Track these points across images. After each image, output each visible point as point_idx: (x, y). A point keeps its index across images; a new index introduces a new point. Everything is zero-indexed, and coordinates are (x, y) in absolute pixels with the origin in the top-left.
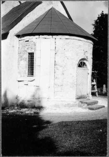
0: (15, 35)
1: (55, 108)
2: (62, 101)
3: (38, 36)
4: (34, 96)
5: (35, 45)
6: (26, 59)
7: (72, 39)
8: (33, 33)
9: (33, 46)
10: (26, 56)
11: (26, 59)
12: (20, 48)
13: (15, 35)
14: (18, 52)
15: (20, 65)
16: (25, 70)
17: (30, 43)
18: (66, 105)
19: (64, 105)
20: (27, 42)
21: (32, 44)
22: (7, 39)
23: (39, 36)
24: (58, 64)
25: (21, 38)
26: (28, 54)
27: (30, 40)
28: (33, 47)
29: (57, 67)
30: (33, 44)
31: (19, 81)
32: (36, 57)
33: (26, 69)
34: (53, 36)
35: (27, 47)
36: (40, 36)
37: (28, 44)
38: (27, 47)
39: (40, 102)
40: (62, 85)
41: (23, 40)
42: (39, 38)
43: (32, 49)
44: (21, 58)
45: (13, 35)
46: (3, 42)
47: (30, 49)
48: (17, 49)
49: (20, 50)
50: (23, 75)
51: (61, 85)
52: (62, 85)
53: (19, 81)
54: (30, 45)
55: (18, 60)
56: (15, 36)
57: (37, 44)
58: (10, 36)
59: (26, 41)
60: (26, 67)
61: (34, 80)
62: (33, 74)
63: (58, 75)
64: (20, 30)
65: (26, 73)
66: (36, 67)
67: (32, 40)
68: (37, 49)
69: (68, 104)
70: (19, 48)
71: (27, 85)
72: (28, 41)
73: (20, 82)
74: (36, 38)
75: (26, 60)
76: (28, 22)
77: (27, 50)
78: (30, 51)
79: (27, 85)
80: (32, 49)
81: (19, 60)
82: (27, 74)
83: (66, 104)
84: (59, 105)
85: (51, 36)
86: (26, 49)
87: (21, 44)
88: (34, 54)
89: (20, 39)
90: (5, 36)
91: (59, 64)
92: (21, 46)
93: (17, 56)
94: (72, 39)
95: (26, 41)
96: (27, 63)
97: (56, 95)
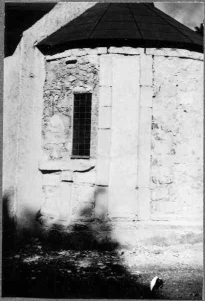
0: (36, 44)
1: (156, 248)
2: (172, 227)
3: (106, 48)
4: (87, 212)
5: (95, 73)
6: (67, 111)
7: (194, 59)
8: (91, 37)
9: (88, 75)
10: (69, 102)
11: (67, 111)
12: (48, 83)
13: (36, 46)
14: (44, 91)
15: (49, 128)
16: (64, 141)
17: (82, 67)
18: (183, 237)
19: (179, 239)
20: (70, 66)
21: (85, 69)
22: (14, 54)
23: (108, 48)
24: (159, 126)
25: (51, 55)
26: (73, 96)
27: (80, 60)
28: (88, 78)
29: (157, 134)
30: (90, 70)
31: (45, 172)
32: (97, 108)
33: (67, 138)
34: (147, 49)
35: (71, 78)
36: (111, 48)
37: (72, 71)
38: (71, 78)
39: (107, 229)
40: (171, 182)
41: (59, 59)
42: (108, 53)
43: (85, 82)
44: (51, 108)
45: (32, 45)
46: (8, 61)
47: (81, 83)
48: (39, 83)
49: (48, 87)
50: (55, 155)
51: (169, 182)
52: (171, 182)
53: (45, 172)
54: (81, 72)
55: (44, 114)
56: (36, 48)
57: (102, 72)
58: (25, 46)
59: (68, 63)
60: (68, 133)
61: (93, 168)
62: (88, 153)
63: (160, 154)
64: (49, 34)
65: (66, 150)
66: (100, 132)
67: (86, 59)
68: (101, 83)
69: (189, 236)
70: (46, 81)
71: (72, 181)
72: (74, 62)
73: (47, 175)
74: (99, 55)
75: (68, 113)
76: (68, 16)
77: (71, 88)
78: (79, 89)
79: (72, 181)
80: (85, 82)
81: (47, 113)
82: (70, 152)
83: (185, 234)
84: (164, 239)
85: (141, 50)
86: (67, 84)
87: (53, 70)
88: (93, 97)
89: (49, 57)
90: (10, 50)
91: (163, 126)
92: (52, 76)
93: (39, 101)
94: (194, 59)
95: (68, 63)
96: (70, 121)
97: (156, 210)
